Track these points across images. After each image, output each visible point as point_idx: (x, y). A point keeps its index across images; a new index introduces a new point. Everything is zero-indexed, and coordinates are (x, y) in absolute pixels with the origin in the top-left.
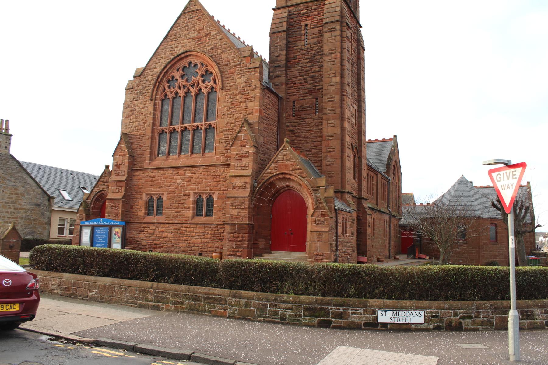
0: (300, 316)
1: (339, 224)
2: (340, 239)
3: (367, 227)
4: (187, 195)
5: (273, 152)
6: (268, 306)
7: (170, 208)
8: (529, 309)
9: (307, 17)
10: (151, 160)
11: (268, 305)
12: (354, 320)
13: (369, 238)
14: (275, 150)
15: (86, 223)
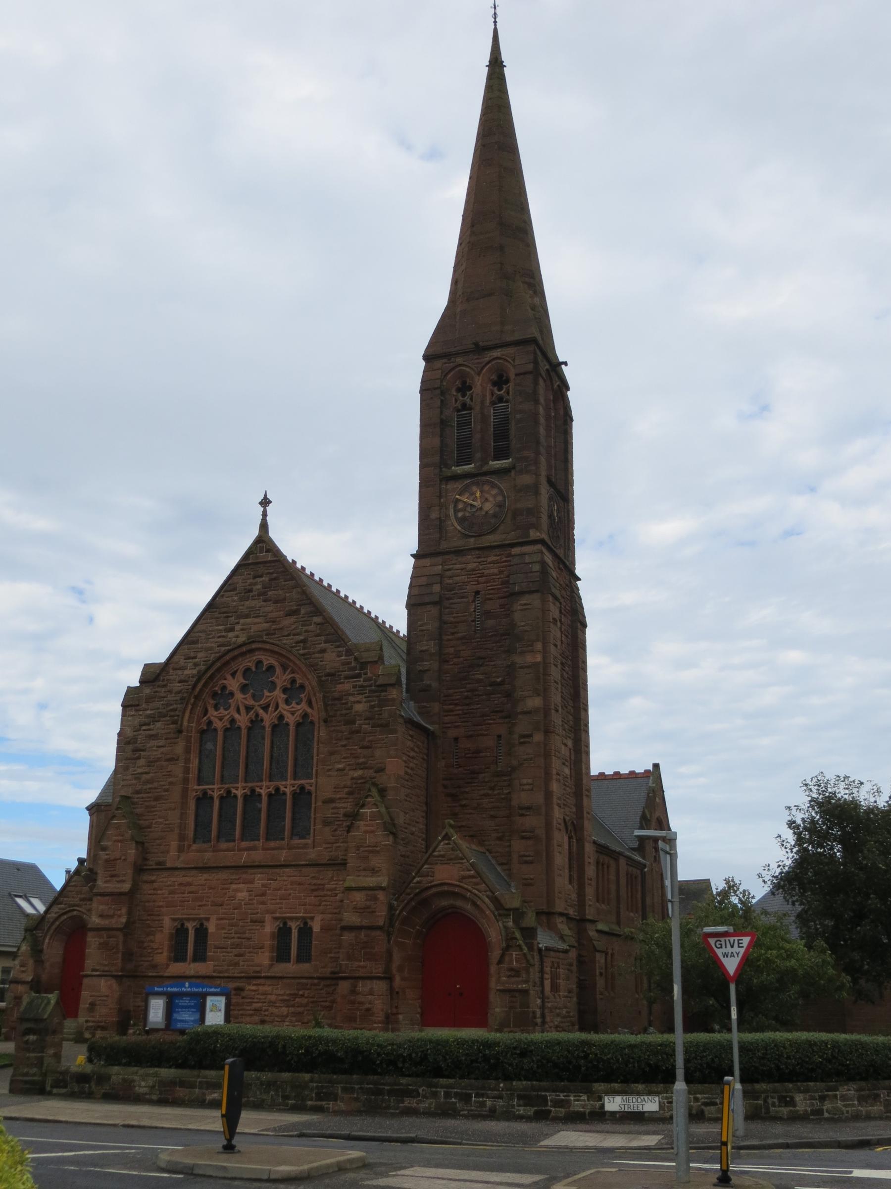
0: (513, 1106)
1: (546, 976)
2: (548, 1002)
3: (597, 978)
4: (259, 922)
5: (419, 837)
6: (473, 1095)
7: (223, 948)
8: (788, 1094)
9: (479, 577)
10: (181, 849)
11: (472, 1094)
12: (577, 1109)
13: (601, 999)
14: (422, 833)
15: (156, 989)
